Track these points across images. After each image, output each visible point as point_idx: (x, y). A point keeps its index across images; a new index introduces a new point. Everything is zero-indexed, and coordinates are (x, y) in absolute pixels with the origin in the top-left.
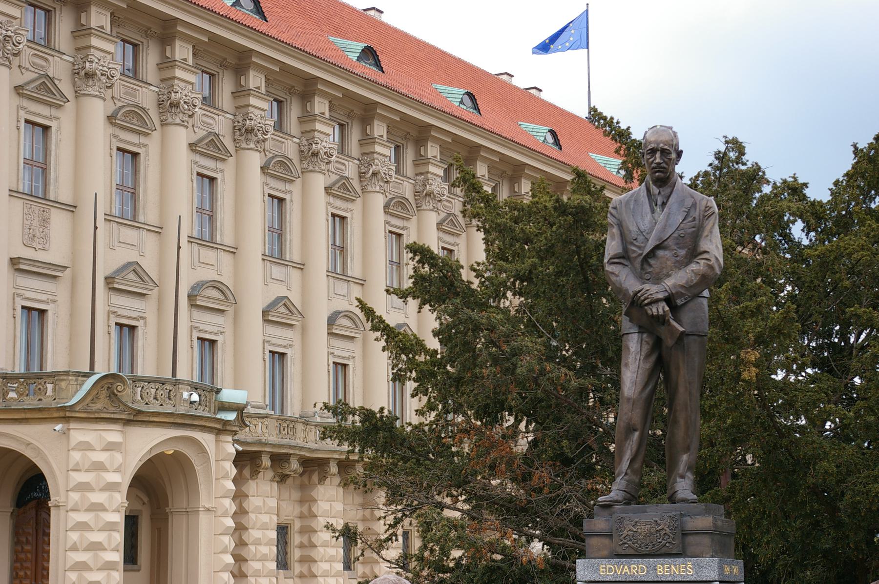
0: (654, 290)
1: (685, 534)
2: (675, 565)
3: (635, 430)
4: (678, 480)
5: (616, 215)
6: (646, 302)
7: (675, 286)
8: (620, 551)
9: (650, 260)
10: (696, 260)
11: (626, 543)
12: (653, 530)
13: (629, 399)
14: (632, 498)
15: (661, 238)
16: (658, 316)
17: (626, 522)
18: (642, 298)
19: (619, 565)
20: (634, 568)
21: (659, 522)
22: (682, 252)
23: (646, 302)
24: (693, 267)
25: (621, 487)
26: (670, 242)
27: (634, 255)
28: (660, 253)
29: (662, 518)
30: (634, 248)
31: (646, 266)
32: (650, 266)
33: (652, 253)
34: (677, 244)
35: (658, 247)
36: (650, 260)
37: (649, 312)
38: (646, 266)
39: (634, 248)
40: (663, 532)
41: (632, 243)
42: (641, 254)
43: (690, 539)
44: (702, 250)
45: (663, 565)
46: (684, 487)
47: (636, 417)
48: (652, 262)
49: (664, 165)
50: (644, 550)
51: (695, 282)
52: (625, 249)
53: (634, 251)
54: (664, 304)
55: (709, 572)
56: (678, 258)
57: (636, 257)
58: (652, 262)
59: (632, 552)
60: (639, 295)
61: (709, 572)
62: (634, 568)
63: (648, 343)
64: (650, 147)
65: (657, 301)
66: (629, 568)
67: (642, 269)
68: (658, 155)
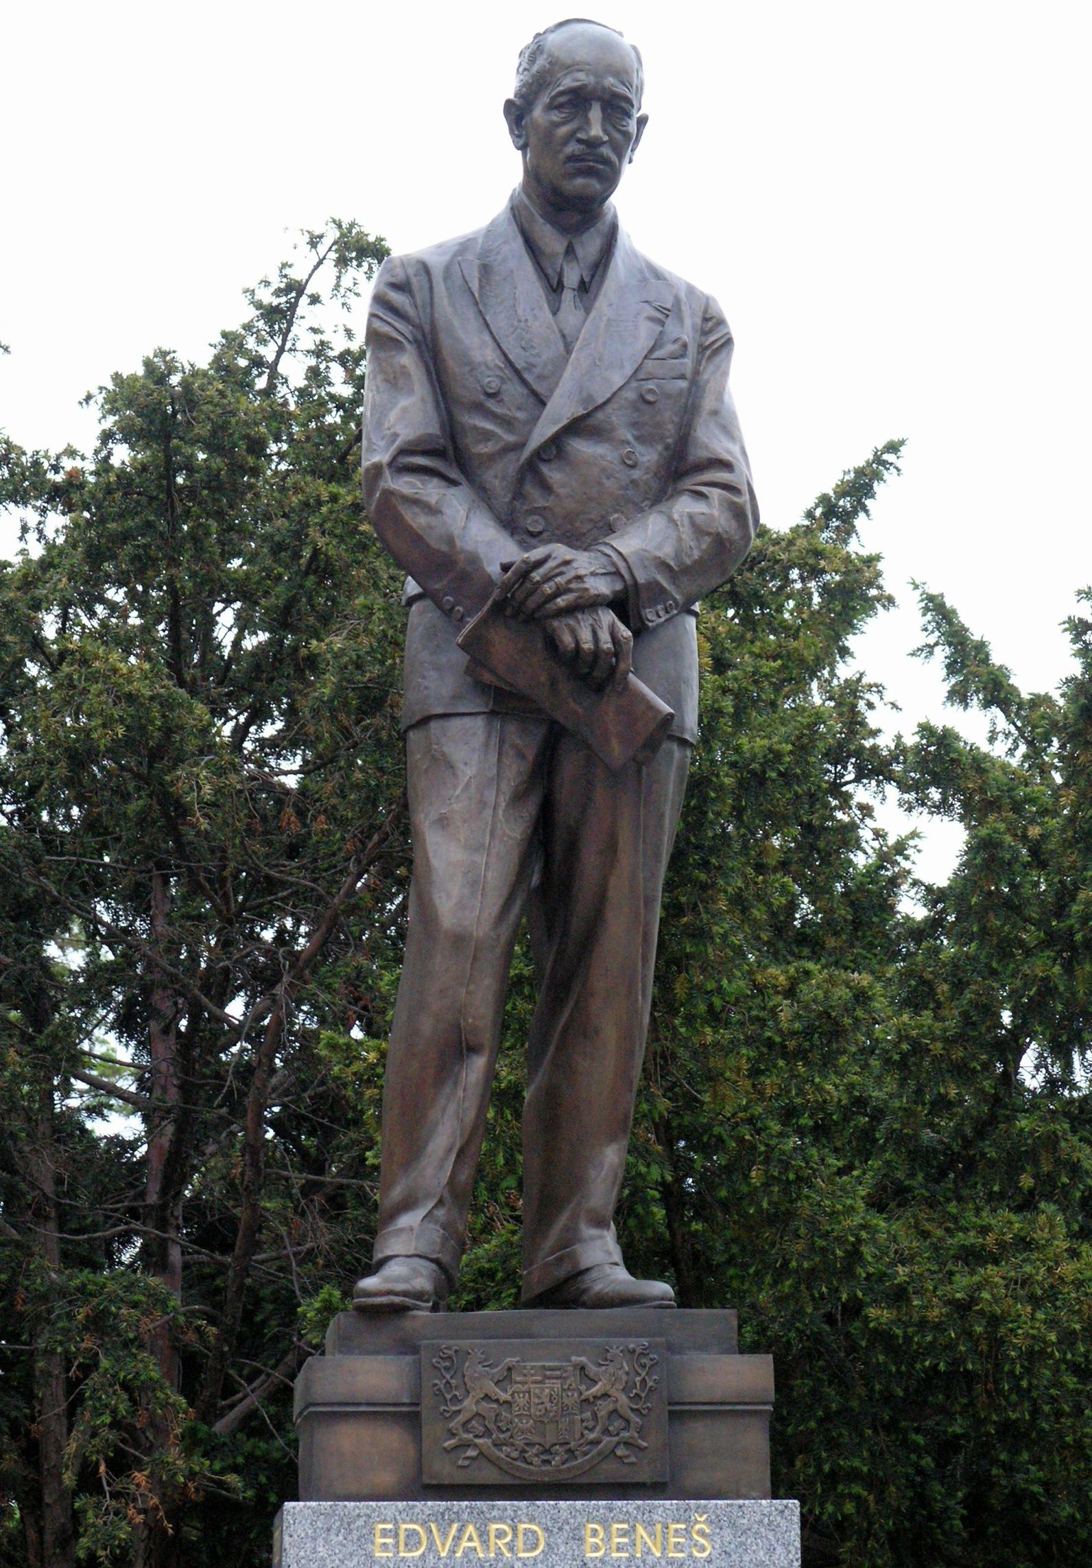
0: (588, 569)
1: (681, 1413)
2: (649, 1524)
3: (474, 1049)
4: (588, 1232)
5: (410, 311)
6: (561, 602)
7: (642, 556)
8: (444, 1470)
9: (545, 469)
10: (688, 483)
11: (466, 1445)
12: (571, 1399)
13: (459, 940)
14: (463, 1288)
15: (590, 398)
16: (597, 653)
17: (472, 1368)
18: (548, 588)
19: (443, 1521)
20: (500, 1535)
21: (592, 1369)
22: (649, 456)
23: (561, 602)
24: (684, 506)
25: (423, 1248)
26: (617, 418)
27: (485, 449)
28: (582, 447)
29: (604, 1356)
30: (488, 426)
31: (531, 490)
32: (546, 487)
33: (555, 447)
34: (634, 424)
35: (576, 427)
36: (545, 469)
37: (567, 639)
38: (531, 490)
39: (488, 426)
40: (604, 1408)
41: (479, 408)
42: (519, 446)
43: (699, 1434)
44: (703, 454)
45: (605, 1523)
46: (602, 1255)
47: (481, 1003)
48: (554, 474)
49: (606, 151)
50: (536, 1470)
51: (696, 555)
52: (451, 428)
53: (487, 436)
54: (608, 617)
55: (771, 1550)
56: (636, 474)
57: (492, 457)
58: (554, 474)
59: (488, 1475)
60: (536, 576)
61: (771, 1550)
62: (500, 1535)
63: (521, 755)
64: (567, 82)
65: (590, 604)
66: (483, 1535)
67: (518, 495)
68: (595, 114)
